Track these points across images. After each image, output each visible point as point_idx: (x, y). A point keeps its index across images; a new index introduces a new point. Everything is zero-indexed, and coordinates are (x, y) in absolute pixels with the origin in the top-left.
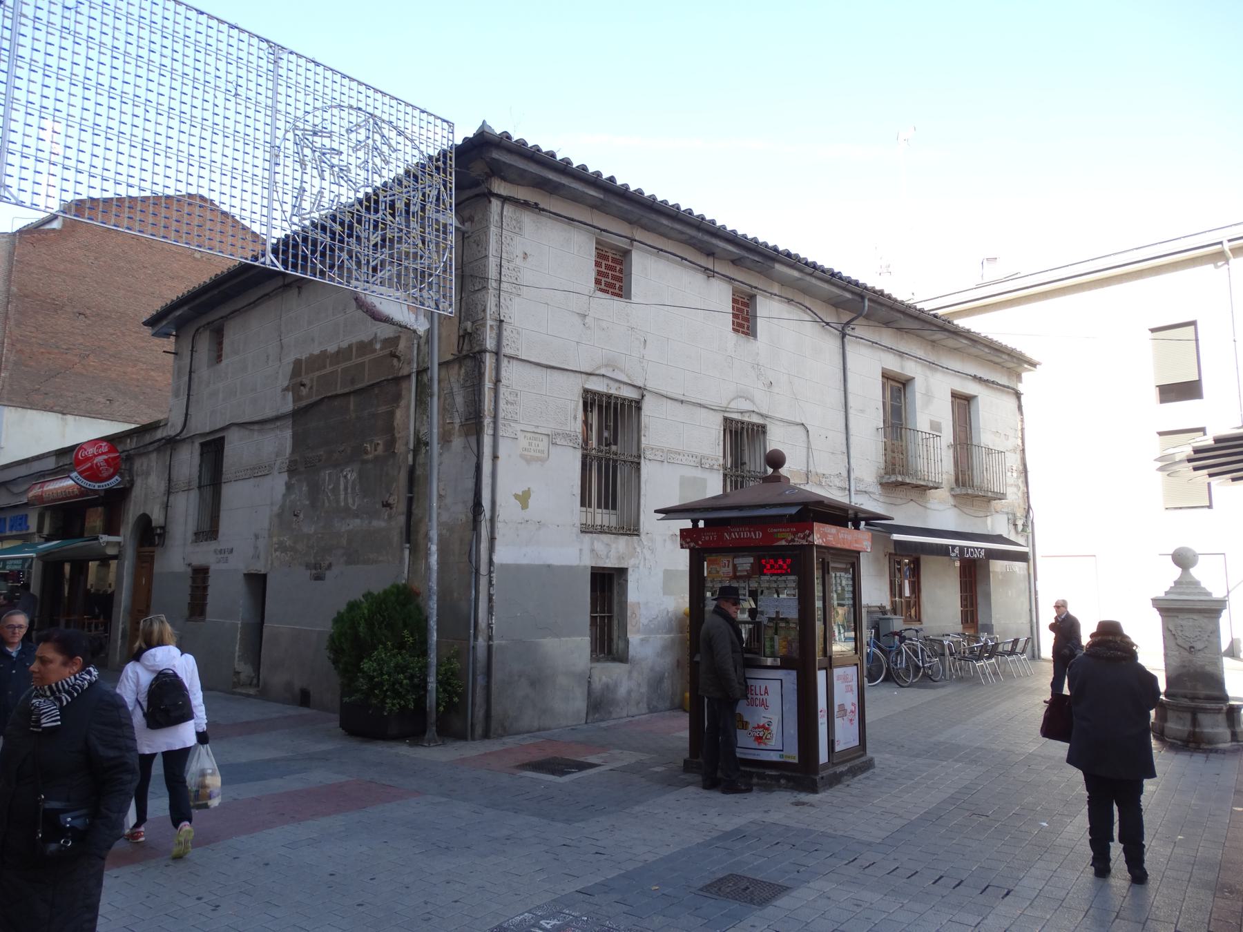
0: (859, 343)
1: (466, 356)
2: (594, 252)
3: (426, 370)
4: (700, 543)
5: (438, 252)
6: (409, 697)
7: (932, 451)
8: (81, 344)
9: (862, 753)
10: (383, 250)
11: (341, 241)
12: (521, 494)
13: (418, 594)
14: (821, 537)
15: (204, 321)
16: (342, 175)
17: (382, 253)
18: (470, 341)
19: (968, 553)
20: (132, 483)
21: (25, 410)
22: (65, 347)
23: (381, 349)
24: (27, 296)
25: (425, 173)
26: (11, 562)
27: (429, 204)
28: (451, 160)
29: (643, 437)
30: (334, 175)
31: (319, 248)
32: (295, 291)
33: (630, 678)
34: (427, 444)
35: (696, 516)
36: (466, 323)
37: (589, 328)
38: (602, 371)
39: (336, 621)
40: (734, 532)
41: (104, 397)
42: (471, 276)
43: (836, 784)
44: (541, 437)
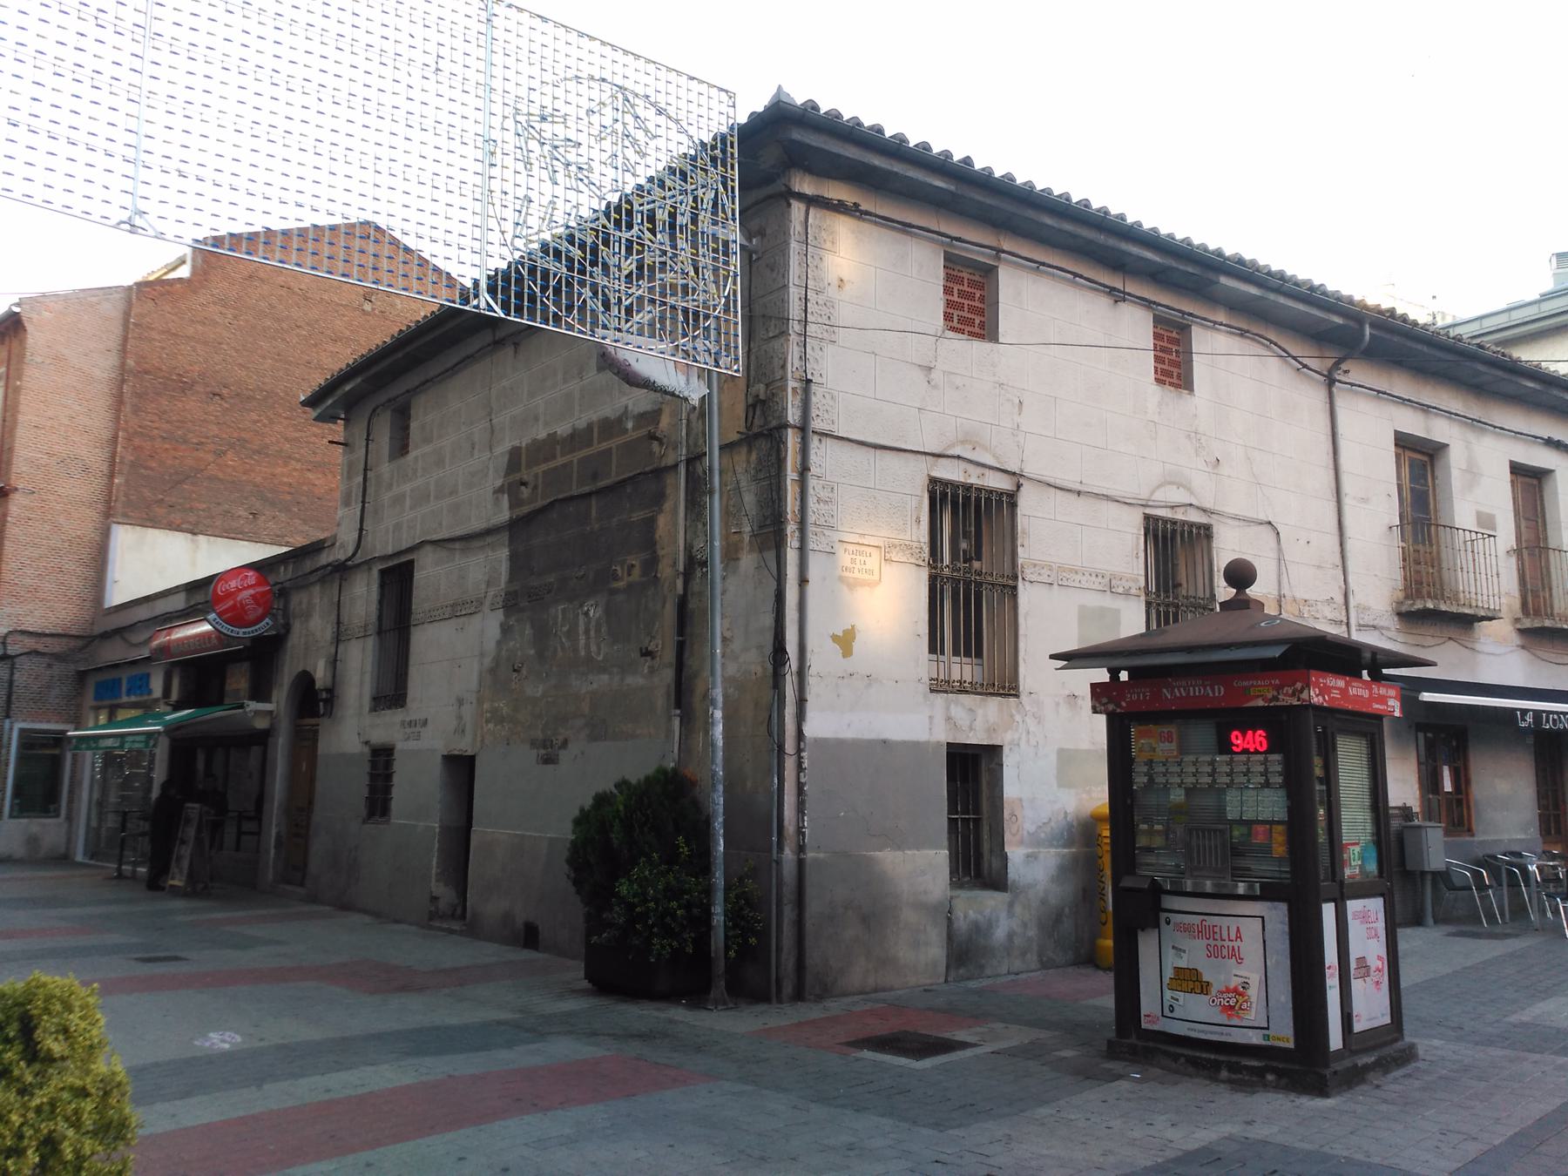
0: (1356, 393)
1: (757, 436)
2: (941, 273)
3: (700, 456)
4: (1124, 704)
5: (716, 282)
6: (686, 936)
7: (1482, 561)
8: (217, 436)
9: (1396, 1035)
10: (640, 283)
11: (582, 272)
12: (841, 634)
13: (693, 784)
14: (1321, 694)
15: (382, 397)
16: (580, 176)
17: (639, 286)
18: (763, 413)
19: (1547, 721)
20: (287, 628)
21: (144, 529)
22: (195, 441)
23: (634, 429)
24: (147, 372)
25: (696, 167)
26: (130, 739)
27: (703, 213)
28: (732, 147)
29: (1020, 550)
30: (570, 177)
31: (552, 283)
32: (510, 350)
33: (1011, 914)
34: (704, 564)
35: (1116, 663)
36: (757, 387)
37: (935, 387)
38: (957, 451)
39: (577, 822)
40: (1179, 688)
41: (246, 510)
42: (764, 316)
43: (1358, 1084)
44: (869, 550)
